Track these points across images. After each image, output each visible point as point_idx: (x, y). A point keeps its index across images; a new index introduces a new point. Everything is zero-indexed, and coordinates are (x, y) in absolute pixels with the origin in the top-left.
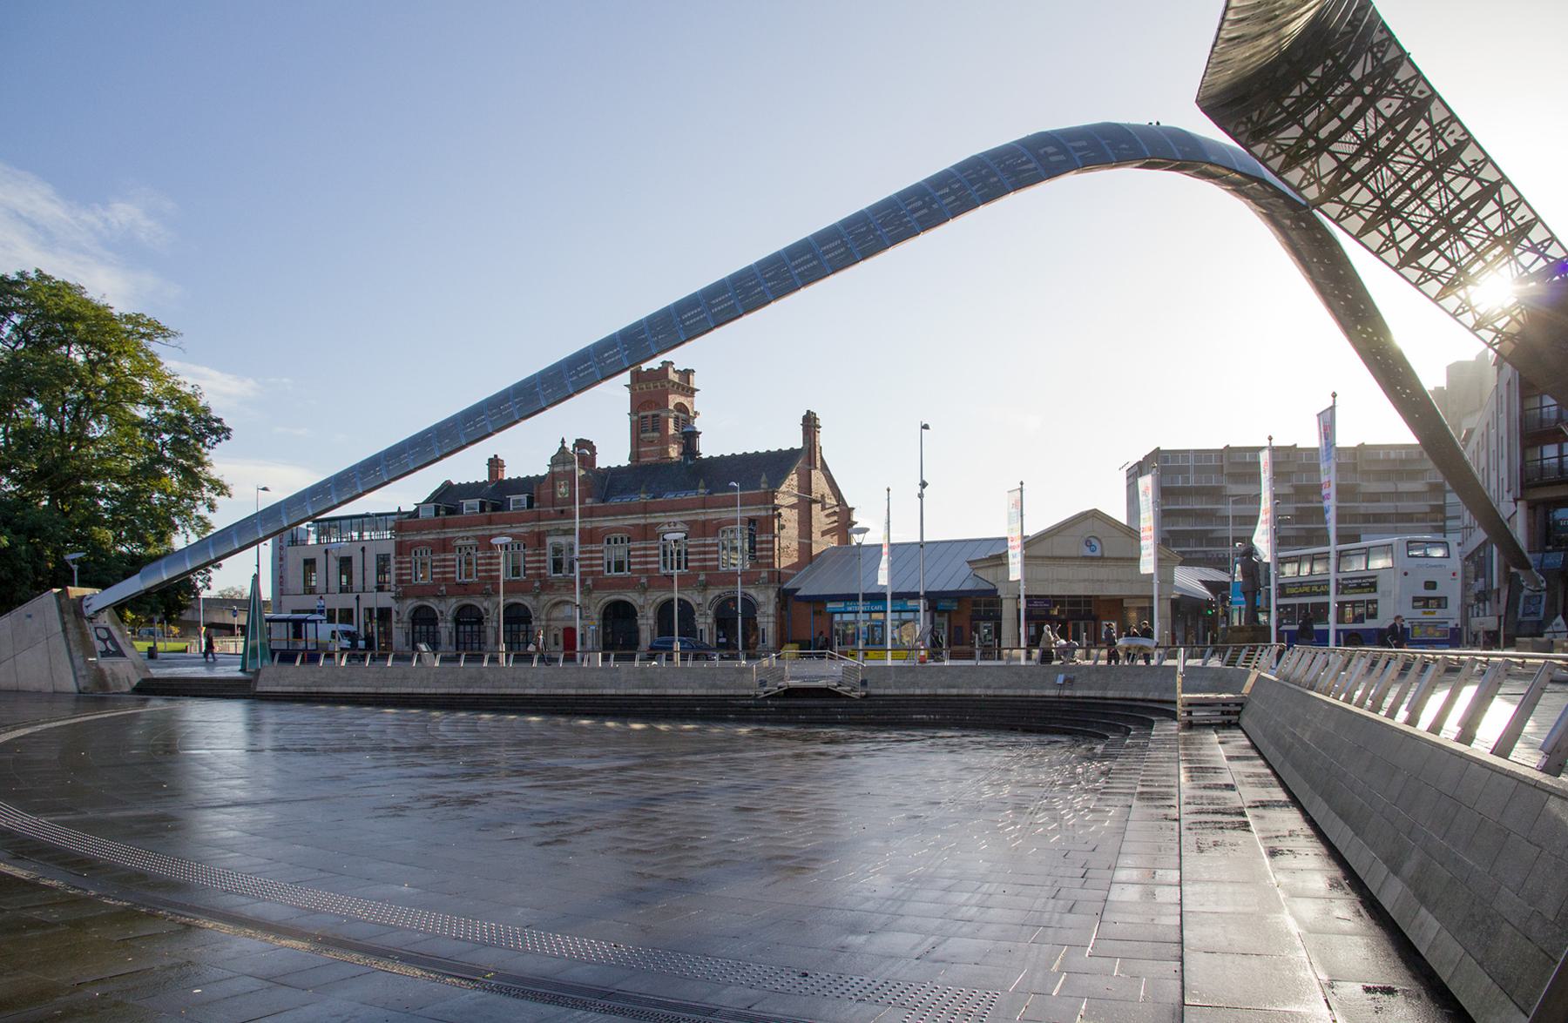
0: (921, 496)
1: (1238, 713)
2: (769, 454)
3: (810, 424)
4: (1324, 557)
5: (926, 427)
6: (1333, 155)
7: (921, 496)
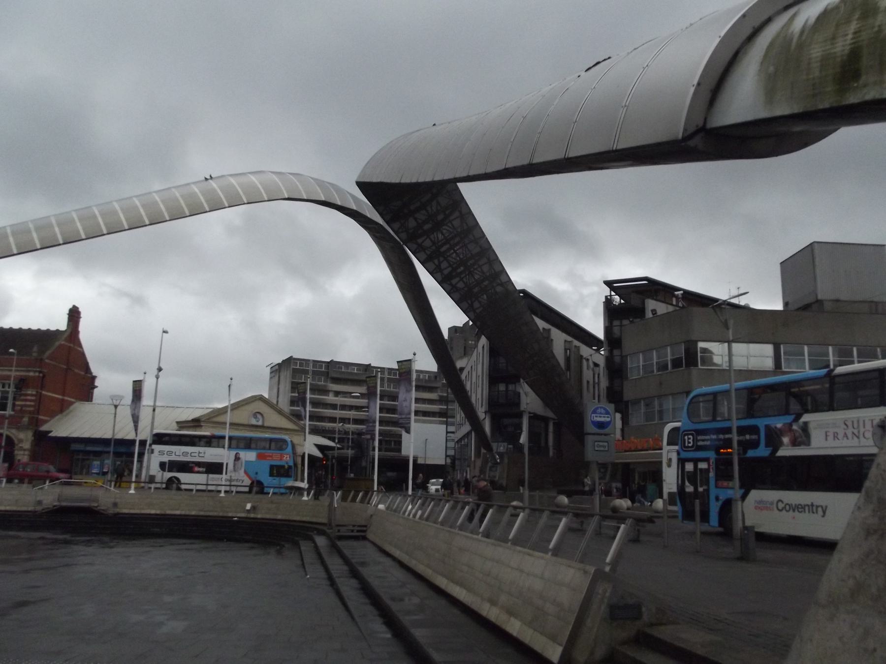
0: (157, 377)
1: (364, 531)
2: (20, 331)
3: (74, 315)
4: (315, 404)
5: (164, 332)
6: (416, 219)
7: (157, 377)
